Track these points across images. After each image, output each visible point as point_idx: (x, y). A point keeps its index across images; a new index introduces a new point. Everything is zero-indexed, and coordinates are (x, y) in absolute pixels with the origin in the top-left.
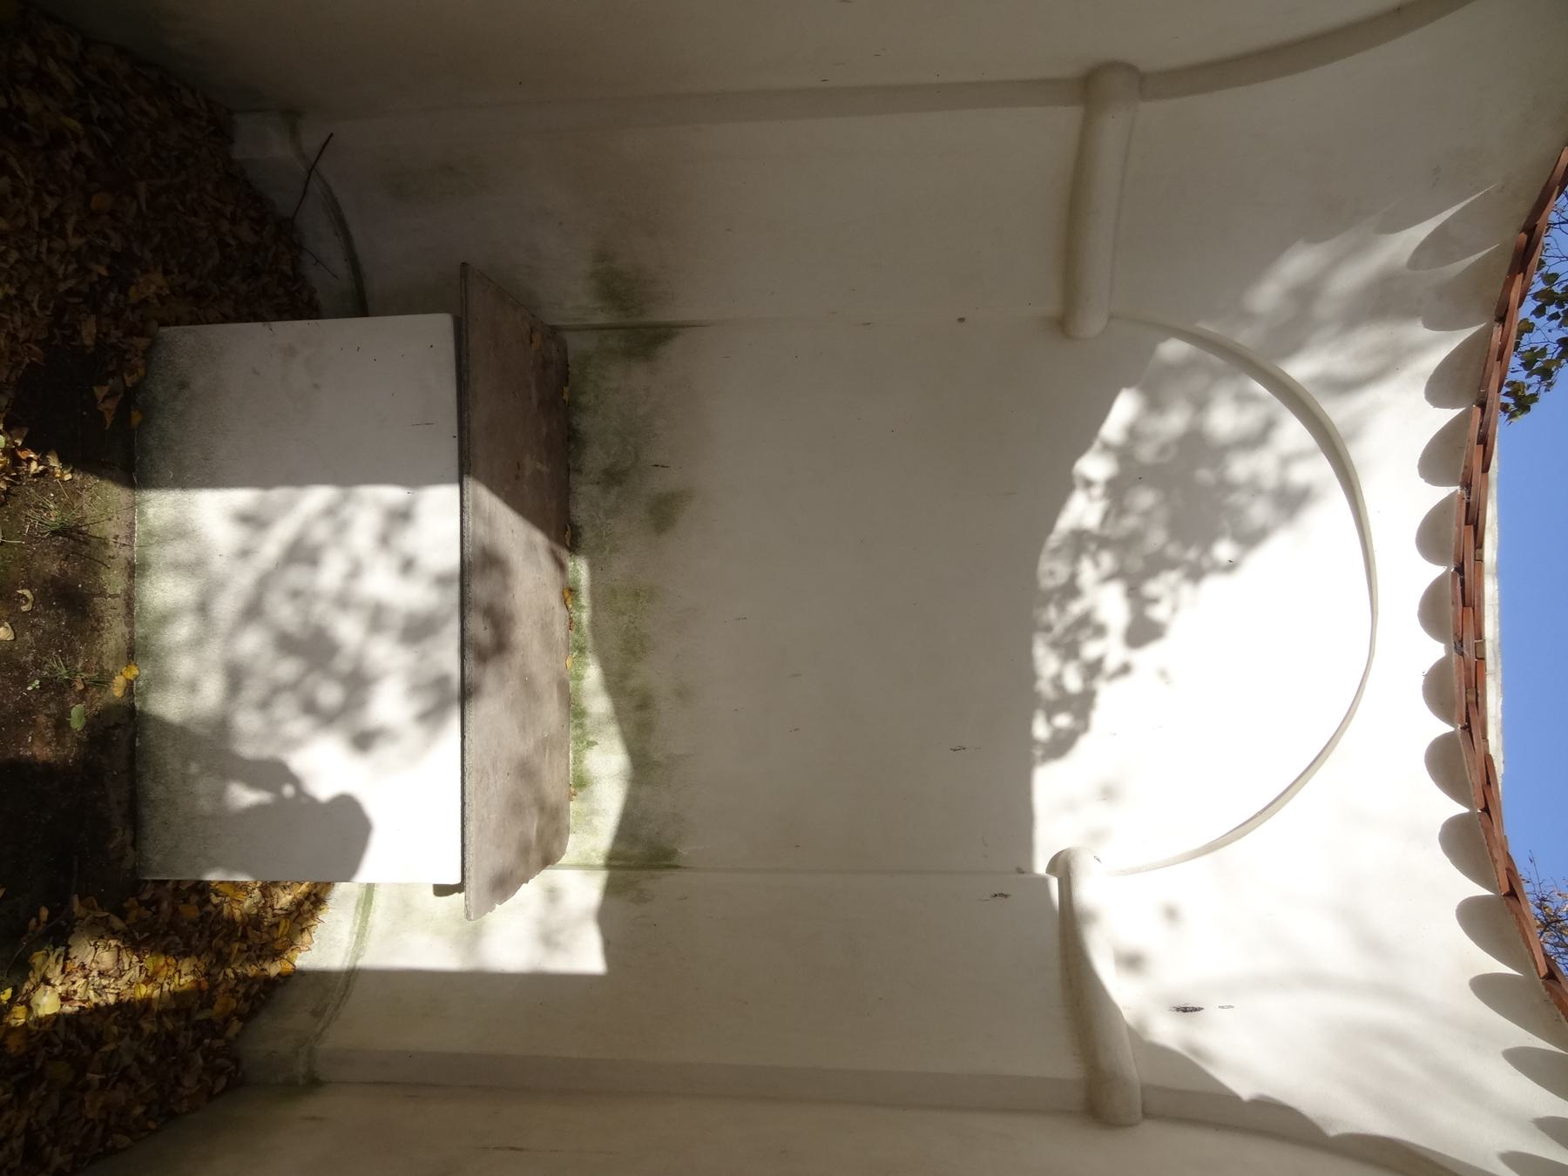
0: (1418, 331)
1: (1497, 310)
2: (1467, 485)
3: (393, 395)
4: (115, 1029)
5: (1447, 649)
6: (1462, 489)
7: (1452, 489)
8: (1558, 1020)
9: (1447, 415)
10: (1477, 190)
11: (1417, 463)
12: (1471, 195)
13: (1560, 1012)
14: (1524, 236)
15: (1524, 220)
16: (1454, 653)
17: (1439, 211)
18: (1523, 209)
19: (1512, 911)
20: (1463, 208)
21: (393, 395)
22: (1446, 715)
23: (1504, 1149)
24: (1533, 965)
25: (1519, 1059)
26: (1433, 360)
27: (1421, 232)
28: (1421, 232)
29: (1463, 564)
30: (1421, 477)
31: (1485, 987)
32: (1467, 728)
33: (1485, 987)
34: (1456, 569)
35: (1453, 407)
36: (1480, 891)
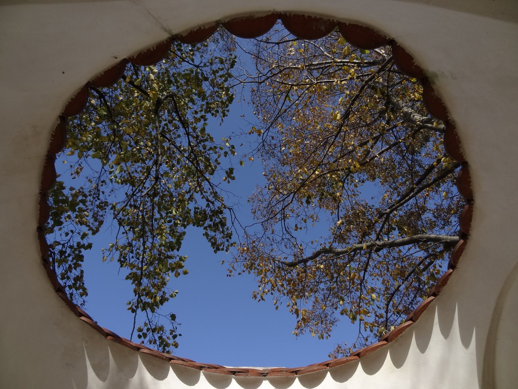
0: (136, 379)
1: (134, 350)
2: (201, 368)
3: (372, 198)
4: (70, 144)
5: (265, 380)
6: (202, 370)
7: (202, 374)
8: (402, 336)
9: (171, 373)
10: (83, 351)
11: (188, 386)
12: (84, 353)
13: (399, 336)
14: (109, 337)
15: (102, 336)
16: (267, 377)
17: (86, 366)
18: (98, 336)
19: (365, 355)
20: (88, 357)
21: (372, 198)
22: (293, 380)
23: (463, 347)
24: (384, 347)
25: (423, 347)
26: (148, 377)
27: (91, 374)
28: (91, 374)
29: (232, 372)
30: (194, 385)
31: (398, 362)
32: (296, 372)
33: (398, 362)
34: (234, 375)
35: (169, 370)
36: (360, 367)
